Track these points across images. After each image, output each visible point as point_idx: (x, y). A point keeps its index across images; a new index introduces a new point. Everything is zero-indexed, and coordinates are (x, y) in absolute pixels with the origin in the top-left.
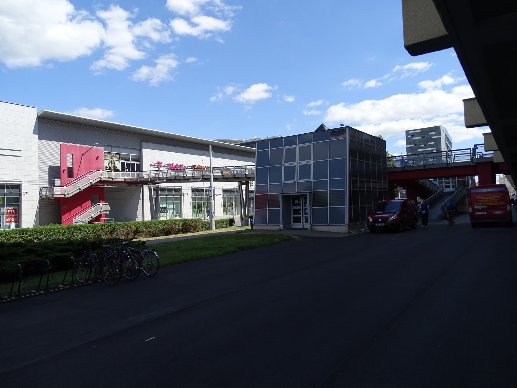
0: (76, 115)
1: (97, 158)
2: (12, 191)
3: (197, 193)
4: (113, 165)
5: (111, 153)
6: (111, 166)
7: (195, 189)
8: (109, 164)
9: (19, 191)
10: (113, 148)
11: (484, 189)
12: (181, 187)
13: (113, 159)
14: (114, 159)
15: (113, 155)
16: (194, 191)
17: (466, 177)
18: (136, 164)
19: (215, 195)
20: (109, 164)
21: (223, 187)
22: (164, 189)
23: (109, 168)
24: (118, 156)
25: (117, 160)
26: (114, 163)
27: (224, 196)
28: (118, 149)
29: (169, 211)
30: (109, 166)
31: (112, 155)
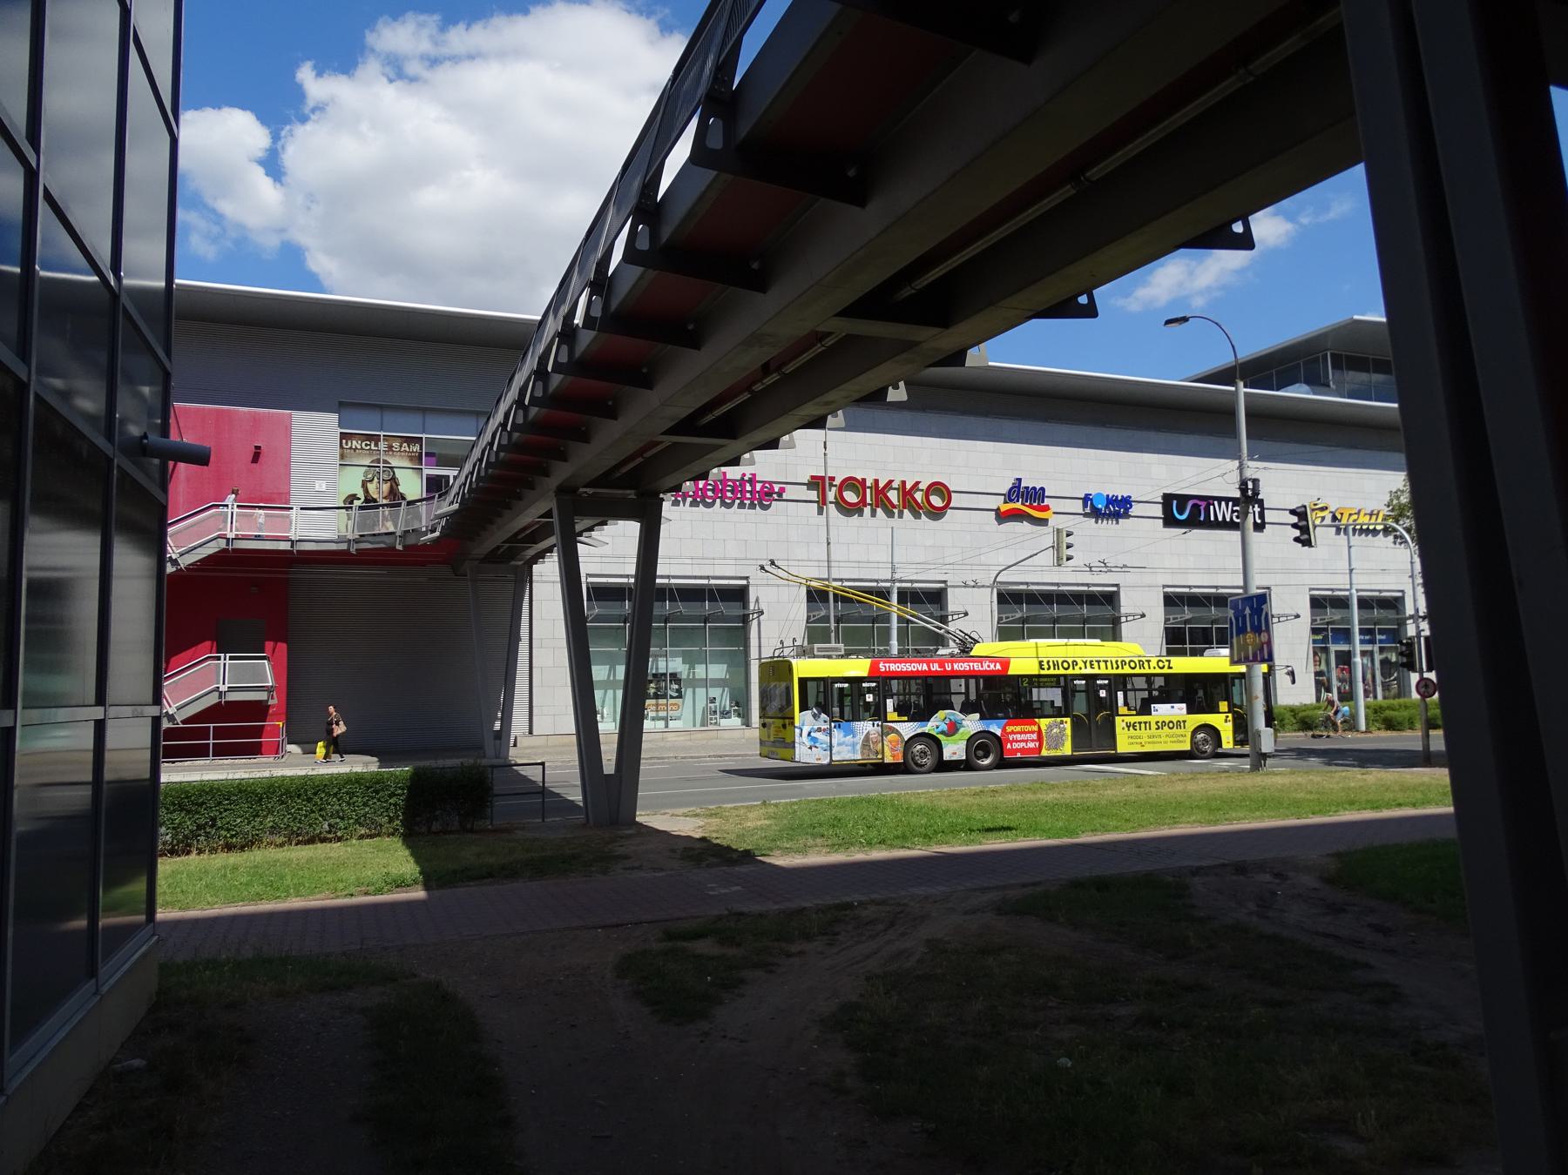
1: (256, 457)
2: (722, 607)
3: (1376, 613)
4: (386, 487)
5: (376, 439)
6: (378, 490)
7: (1325, 598)
8: (369, 485)
9: (744, 608)
10: (389, 417)
11: (32, 6)
12: (1115, 589)
13: (385, 462)
14: (394, 462)
15: (390, 447)
16: (1176, 605)
19: (1275, 620)
20: (369, 485)
21: (1313, 587)
22: (1205, 597)
23: (367, 501)
24: (416, 448)
25: (407, 464)
26: (394, 481)
27: (1172, 621)
28: (416, 419)
29: (694, 693)
30: (366, 491)
31: (382, 445)
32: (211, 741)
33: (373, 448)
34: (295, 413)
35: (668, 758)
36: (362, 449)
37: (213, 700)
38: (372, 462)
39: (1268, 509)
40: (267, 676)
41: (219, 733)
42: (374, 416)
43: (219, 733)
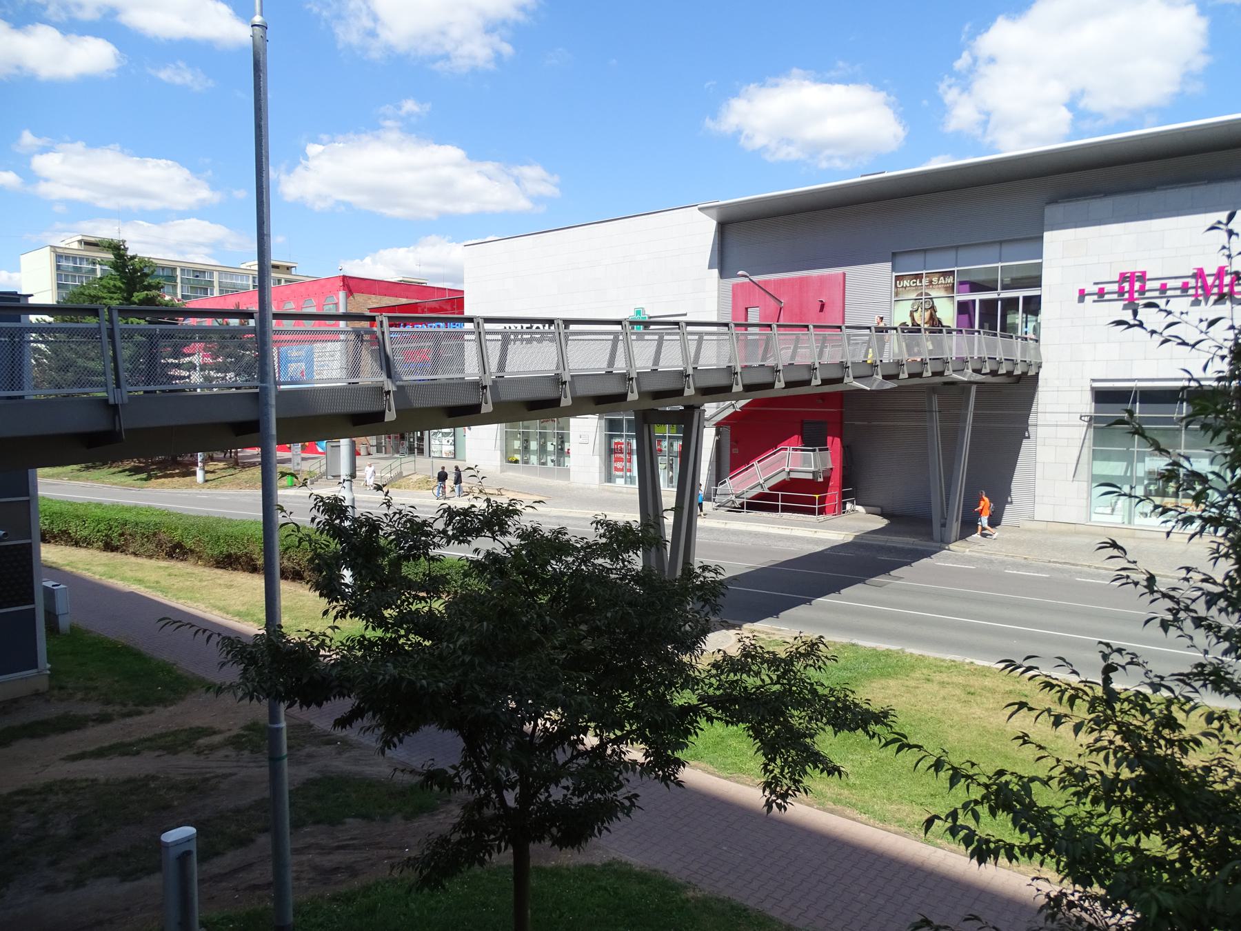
0: (1155, 126)
1: (822, 309)
4: (927, 314)
6: (921, 318)
10: (931, 257)
13: (927, 294)
14: (933, 294)
15: (931, 282)
17: (50, 553)
18: (981, 301)
20: (915, 314)
24: (950, 280)
25: (943, 293)
26: (933, 308)
30: (913, 319)
31: (925, 281)
32: (780, 503)
33: (918, 284)
34: (851, 271)
35: (1082, 565)
36: (910, 286)
37: (783, 477)
38: (917, 296)
39: (657, 360)
40: (1113, 447)
41: (785, 499)
42: (919, 258)
43: (785, 499)
